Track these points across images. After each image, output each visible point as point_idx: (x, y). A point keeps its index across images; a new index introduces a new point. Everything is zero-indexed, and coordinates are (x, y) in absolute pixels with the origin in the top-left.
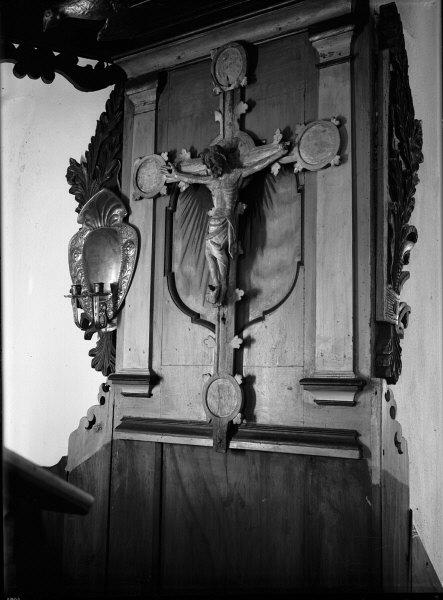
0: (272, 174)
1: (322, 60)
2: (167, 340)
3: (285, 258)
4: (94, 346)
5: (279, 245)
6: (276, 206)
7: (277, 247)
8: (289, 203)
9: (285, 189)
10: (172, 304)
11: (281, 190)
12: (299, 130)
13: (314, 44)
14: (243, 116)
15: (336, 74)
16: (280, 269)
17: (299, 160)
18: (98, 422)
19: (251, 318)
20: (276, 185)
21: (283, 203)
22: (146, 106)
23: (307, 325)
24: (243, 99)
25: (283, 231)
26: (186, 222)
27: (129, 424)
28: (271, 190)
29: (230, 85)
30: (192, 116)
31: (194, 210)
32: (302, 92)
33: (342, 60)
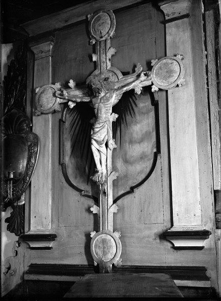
0: (136, 94)
1: (167, 18)
2: (62, 209)
3: (146, 150)
4: (9, 215)
5: (141, 141)
6: (137, 114)
7: (139, 143)
8: (148, 113)
9: (144, 104)
10: (66, 184)
11: (141, 105)
12: (153, 62)
13: (161, 7)
14: (95, 69)
15: (178, 27)
16: (143, 157)
17: (57, 103)
18: (13, 268)
19: (174, 242)
20: (137, 102)
21: (142, 113)
22: (43, 54)
23: (67, 125)
24: (95, 62)
25: (144, 132)
26: (75, 126)
27: (35, 269)
28: (134, 105)
29: (102, 37)
30: (76, 59)
31: (78, 122)
32: (154, 39)
33: (187, 16)
